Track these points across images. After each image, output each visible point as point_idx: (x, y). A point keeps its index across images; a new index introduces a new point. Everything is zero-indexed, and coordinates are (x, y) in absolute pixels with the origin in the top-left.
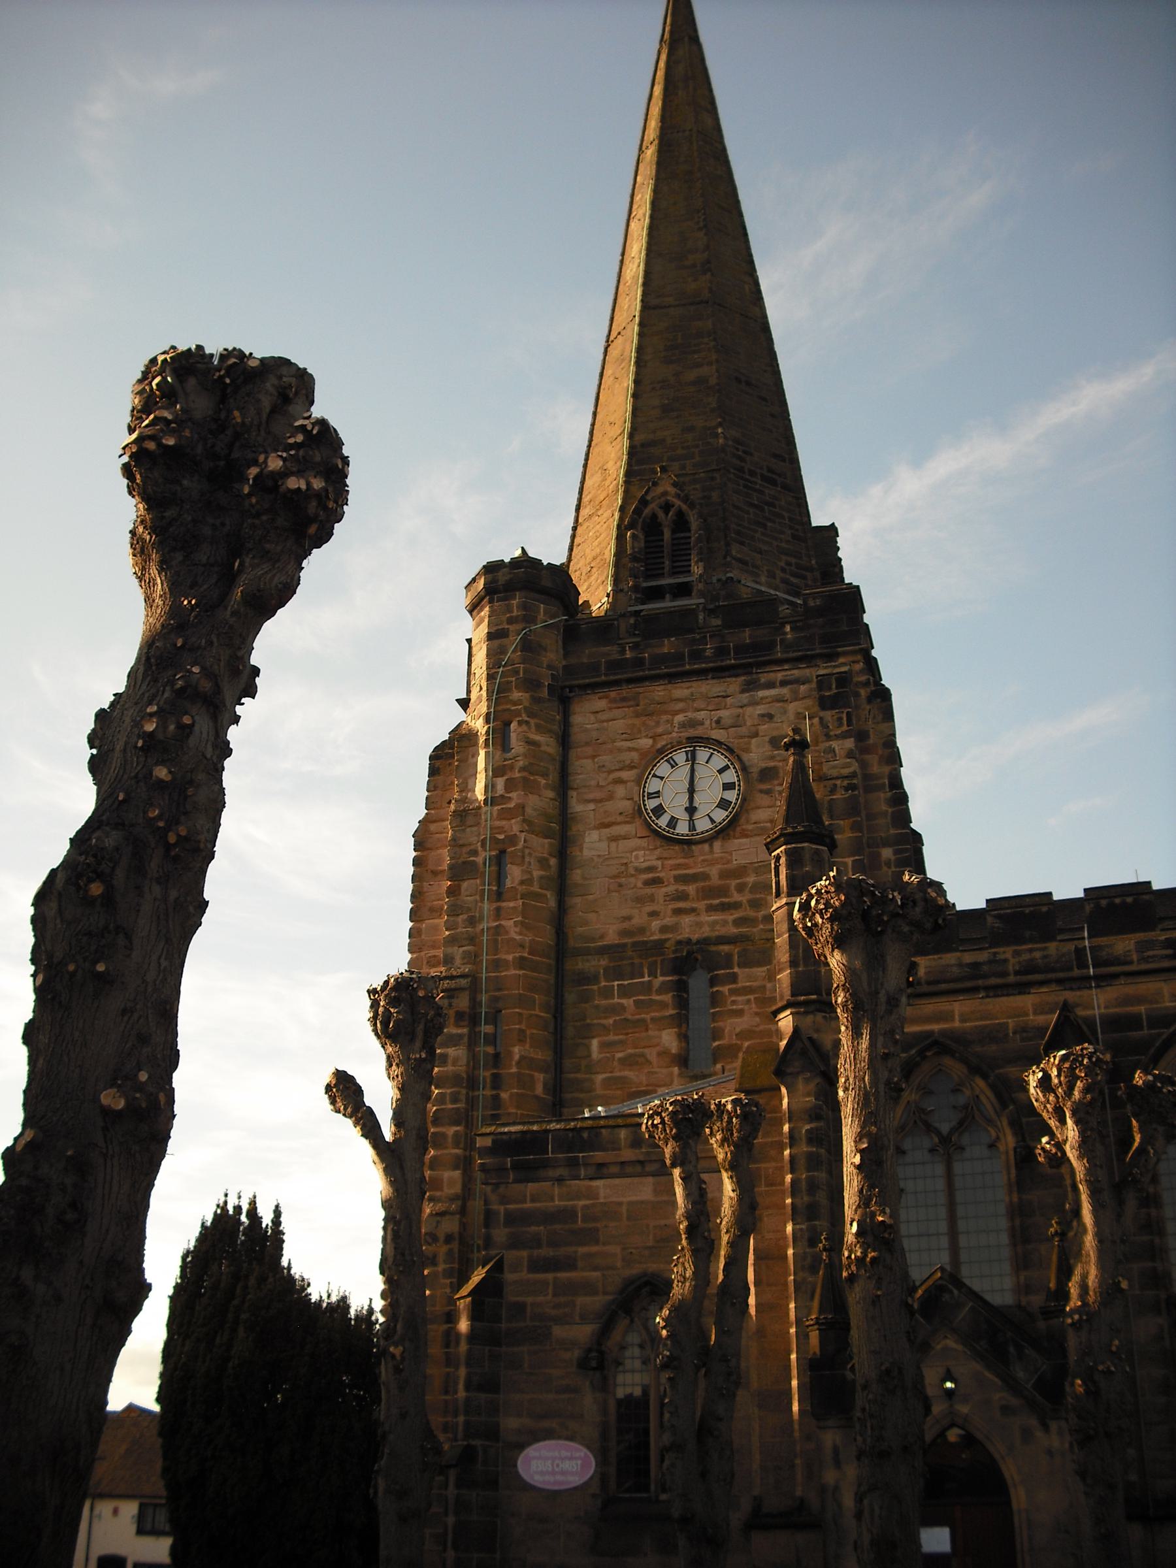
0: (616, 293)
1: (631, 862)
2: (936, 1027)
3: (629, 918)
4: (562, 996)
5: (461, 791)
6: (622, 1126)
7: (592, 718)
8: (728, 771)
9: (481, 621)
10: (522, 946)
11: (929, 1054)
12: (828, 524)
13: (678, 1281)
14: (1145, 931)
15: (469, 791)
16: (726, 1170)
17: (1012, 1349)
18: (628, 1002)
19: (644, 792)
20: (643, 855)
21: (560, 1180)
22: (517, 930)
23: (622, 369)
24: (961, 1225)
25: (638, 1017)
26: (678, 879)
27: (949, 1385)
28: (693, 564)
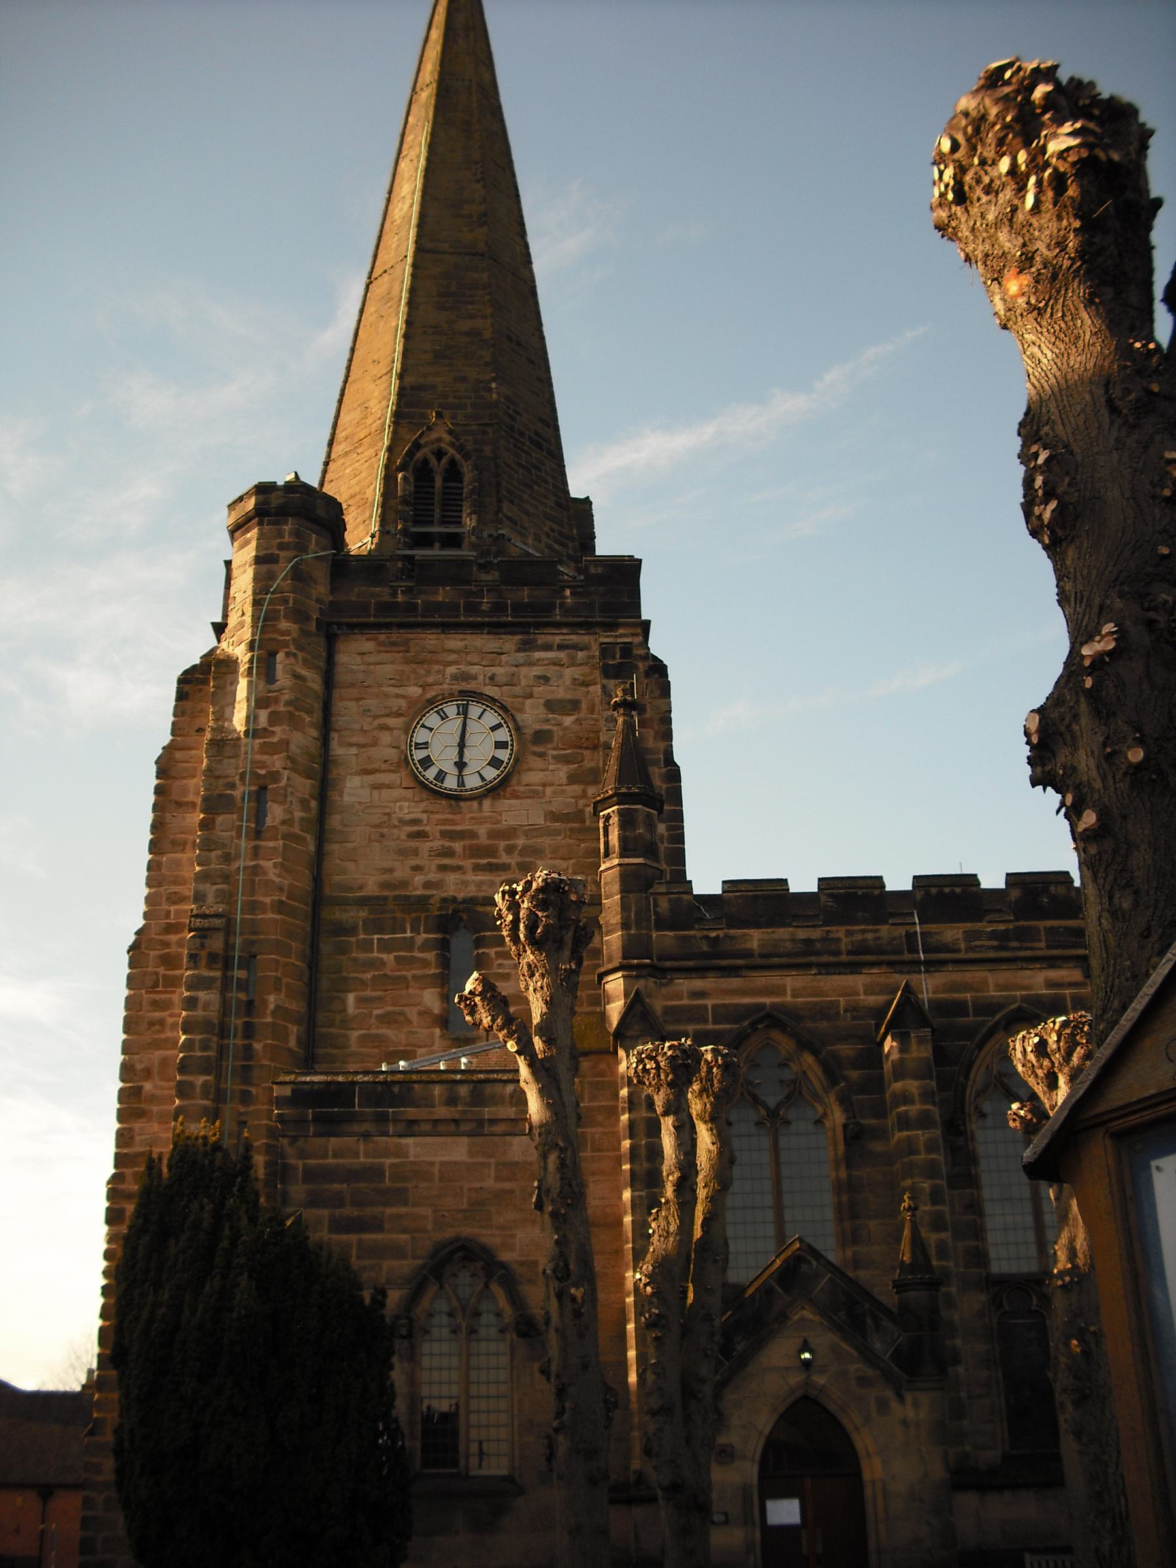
0: (381, 231)
1: (394, 813)
2: (767, 1000)
3: (391, 870)
4: (318, 946)
5: (216, 720)
6: (436, 1082)
7: (359, 659)
8: (501, 730)
9: (247, 542)
10: (281, 889)
11: (760, 1026)
12: (582, 497)
13: (660, 1236)
14: (972, 921)
15: (226, 720)
16: (705, 1122)
17: (869, 1321)
18: (389, 958)
19: (411, 741)
20: (408, 807)
21: (366, 1136)
22: (277, 871)
23: (390, 307)
24: (787, 1200)
25: (397, 973)
26: (445, 834)
27: (807, 1355)
28: (464, 516)
